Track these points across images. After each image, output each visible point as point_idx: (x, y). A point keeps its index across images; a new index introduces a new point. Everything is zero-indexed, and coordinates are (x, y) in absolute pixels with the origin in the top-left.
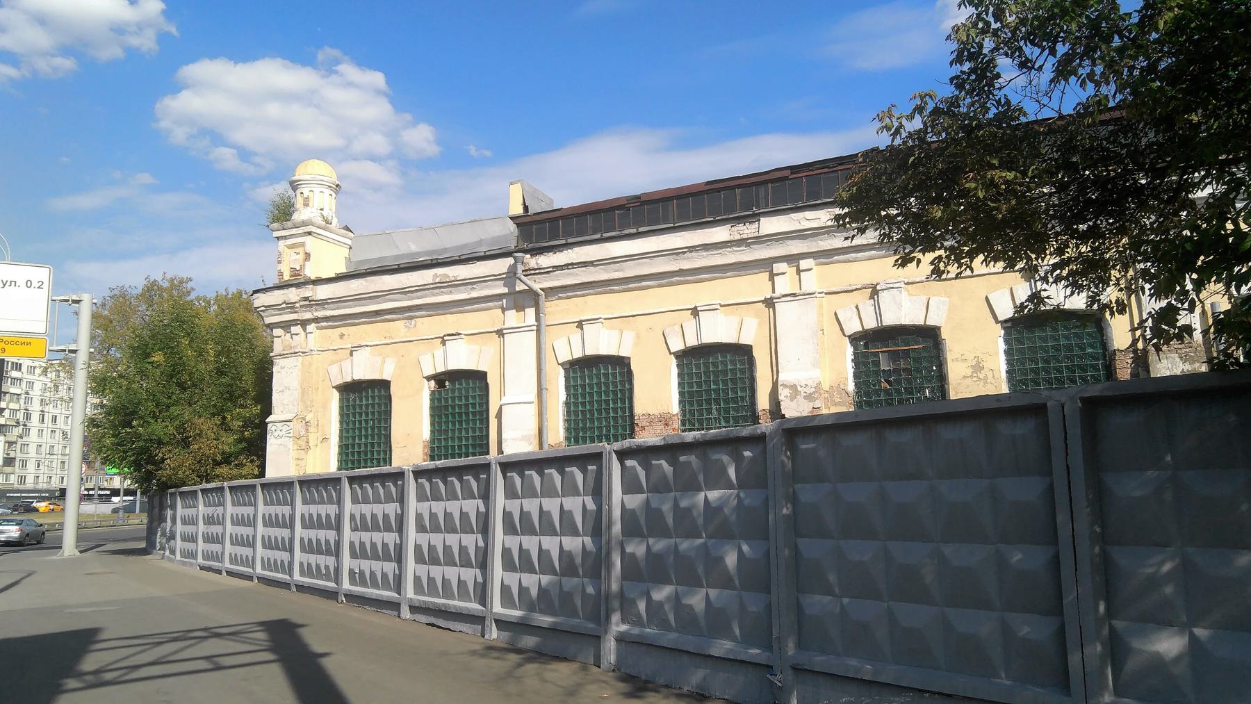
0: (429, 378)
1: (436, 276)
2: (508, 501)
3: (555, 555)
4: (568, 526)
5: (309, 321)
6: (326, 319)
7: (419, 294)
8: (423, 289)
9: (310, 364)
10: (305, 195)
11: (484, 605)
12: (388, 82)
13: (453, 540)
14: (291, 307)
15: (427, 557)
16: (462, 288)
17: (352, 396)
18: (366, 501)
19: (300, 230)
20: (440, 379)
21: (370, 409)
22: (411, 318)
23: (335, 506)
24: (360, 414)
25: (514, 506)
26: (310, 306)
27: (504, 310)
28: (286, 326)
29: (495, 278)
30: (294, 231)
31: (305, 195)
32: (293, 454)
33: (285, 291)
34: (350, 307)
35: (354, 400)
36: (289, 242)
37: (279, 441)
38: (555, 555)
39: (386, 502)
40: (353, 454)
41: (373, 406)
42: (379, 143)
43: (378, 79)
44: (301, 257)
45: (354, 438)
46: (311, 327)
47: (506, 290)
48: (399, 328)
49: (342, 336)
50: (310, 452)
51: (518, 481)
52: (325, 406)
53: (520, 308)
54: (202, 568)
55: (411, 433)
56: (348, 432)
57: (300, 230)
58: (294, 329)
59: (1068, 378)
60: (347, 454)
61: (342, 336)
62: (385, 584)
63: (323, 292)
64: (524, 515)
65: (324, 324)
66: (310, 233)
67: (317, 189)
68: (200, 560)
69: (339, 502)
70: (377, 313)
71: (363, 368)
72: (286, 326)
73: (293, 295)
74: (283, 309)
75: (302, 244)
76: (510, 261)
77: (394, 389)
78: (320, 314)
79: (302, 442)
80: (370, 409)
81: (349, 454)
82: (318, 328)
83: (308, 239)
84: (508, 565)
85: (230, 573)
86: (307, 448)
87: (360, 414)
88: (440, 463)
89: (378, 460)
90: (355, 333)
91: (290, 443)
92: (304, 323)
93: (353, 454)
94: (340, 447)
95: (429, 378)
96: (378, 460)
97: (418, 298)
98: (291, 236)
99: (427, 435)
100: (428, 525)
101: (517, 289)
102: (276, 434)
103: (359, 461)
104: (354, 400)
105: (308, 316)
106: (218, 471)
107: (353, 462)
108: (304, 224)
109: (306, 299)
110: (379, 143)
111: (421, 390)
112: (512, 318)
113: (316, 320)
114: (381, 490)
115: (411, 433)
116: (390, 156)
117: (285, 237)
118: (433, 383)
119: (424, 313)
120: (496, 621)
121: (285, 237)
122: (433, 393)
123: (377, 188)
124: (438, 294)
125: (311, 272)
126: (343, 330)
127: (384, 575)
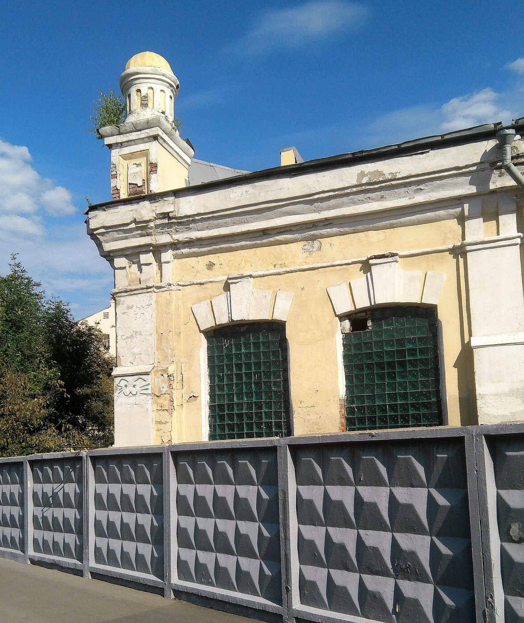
0: (342, 318)
1: (362, 174)
2: (98, 485)
3: (61, 520)
4: (242, 511)
5: (165, 247)
6: (190, 243)
7: (333, 202)
8: (341, 194)
9: (169, 303)
10: (143, 93)
11: (81, 560)
12: (30, 151)
13: (129, 518)
14: (142, 227)
15: (106, 531)
16: (402, 190)
17: (226, 343)
18: (47, 480)
19: (143, 134)
20: (358, 320)
21: (253, 359)
22: (313, 238)
23: (18, 486)
24: (239, 367)
25: (103, 489)
26: (169, 225)
27: (462, 219)
28: (133, 254)
29: (458, 172)
30: (134, 136)
31: (143, 93)
32: (153, 416)
33: (135, 206)
34: (226, 225)
35: (229, 349)
36: (126, 150)
37: (132, 399)
38: (61, 520)
39: (45, 483)
40: (231, 417)
41: (257, 355)
42: (24, 201)
43: (24, 150)
44: (143, 169)
45: (230, 396)
46: (167, 256)
47: (473, 190)
48: (295, 253)
49: (210, 266)
50: (175, 413)
51: (40, 474)
52: (190, 356)
53: (491, 215)
54: (34, 562)
55: (319, 392)
56: (221, 388)
57: (143, 134)
58: (145, 258)
59: (380, 417)
60: (222, 418)
61: (210, 266)
62: (67, 551)
63: (189, 206)
64: (111, 496)
65: (186, 251)
66: (155, 138)
67: (158, 87)
68: (31, 551)
69: (22, 483)
70: (265, 232)
71: (248, 305)
72: (133, 254)
73: (146, 210)
74: (131, 230)
75: (145, 153)
76: (490, 144)
77: (291, 333)
78: (182, 236)
79: (164, 402)
80: (253, 359)
81: (223, 417)
82: (176, 257)
83: (154, 147)
84: (99, 533)
85: (96, 575)
86: (170, 410)
87: (239, 367)
88: (356, 435)
89: (269, 426)
90: (228, 263)
91: (149, 403)
92: (157, 250)
93: (231, 417)
94: (211, 408)
95: (342, 318)
96: (269, 426)
97: (329, 208)
98: (129, 143)
99: (342, 391)
100: (105, 503)
101: (492, 187)
102: (127, 391)
103: (240, 427)
104: (229, 349)
105: (165, 239)
106: (35, 439)
107: (231, 427)
108: (148, 125)
109: (166, 215)
110: (24, 201)
111: (331, 334)
112: (477, 229)
113: (174, 246)
114: (40, 474)
115: (319, 392)
116: (37, 213)
117: (121, 145)
118: (347, 324)
119: (335, 230)
120: (174, 591)
121: (121, 145)
122: (346, 337)
123: (29, 237)
124: (362, 202)
125: (157, 186)
126: (212, 258)
127: (12, 538)
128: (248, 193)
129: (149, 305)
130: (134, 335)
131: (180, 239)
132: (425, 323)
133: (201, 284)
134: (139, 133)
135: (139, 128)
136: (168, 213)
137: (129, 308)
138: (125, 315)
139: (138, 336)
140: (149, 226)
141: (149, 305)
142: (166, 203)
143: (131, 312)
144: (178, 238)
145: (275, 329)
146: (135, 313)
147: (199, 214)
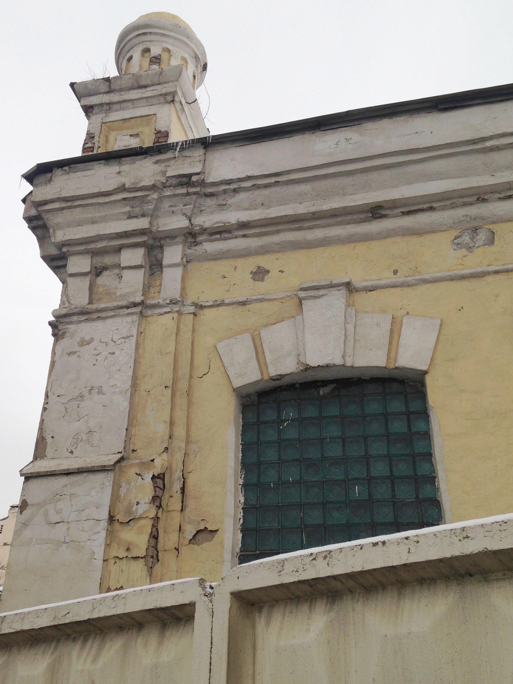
49: (260, 274)
77: (437, 394)
126: (263, 261)
128: (350, 141)
129: (128, 337)
130: (86, 394)
131: (207, 225)
132: (286, 562)
133: (244, 303)
134: (144, 90)
135: (143, 83)
136: (190, 176)
137: (83, 343)
138: (74, 357)
139: (96, 397)
140: (150, 198)
141: (128, 337)
142: (188, 160)
143: (87, 351)
144: (201, 223)
145: (404, 389)
146: (95, 352)
147: (249, 178)
